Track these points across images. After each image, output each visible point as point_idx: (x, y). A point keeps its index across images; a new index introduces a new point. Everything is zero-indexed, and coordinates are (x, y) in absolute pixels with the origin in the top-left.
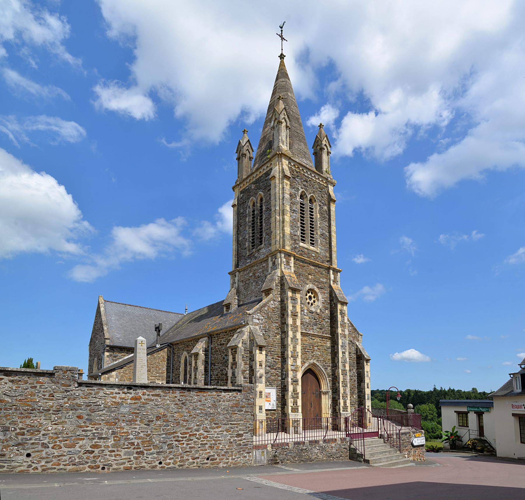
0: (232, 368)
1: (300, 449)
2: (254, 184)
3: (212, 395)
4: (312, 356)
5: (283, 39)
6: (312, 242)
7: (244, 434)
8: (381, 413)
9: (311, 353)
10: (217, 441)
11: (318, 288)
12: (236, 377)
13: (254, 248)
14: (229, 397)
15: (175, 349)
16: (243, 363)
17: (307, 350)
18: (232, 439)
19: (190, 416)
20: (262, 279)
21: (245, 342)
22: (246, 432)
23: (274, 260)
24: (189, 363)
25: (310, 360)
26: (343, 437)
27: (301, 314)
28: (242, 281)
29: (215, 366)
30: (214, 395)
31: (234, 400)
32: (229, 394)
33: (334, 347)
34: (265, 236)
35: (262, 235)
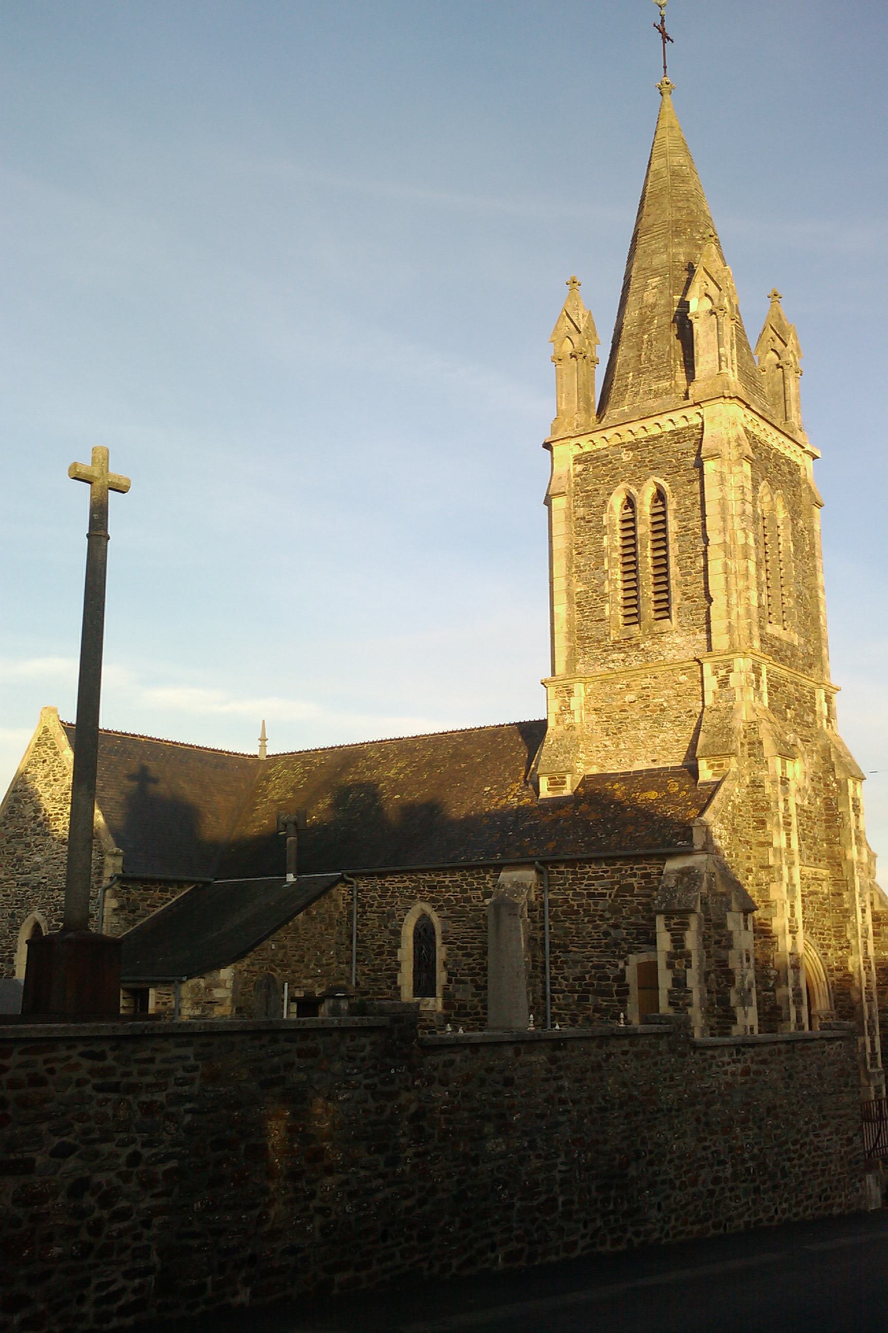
2: (631, 449)
5: (666, 37)
12: (691, 992)
23: (722, 673)
33: (840, 895)
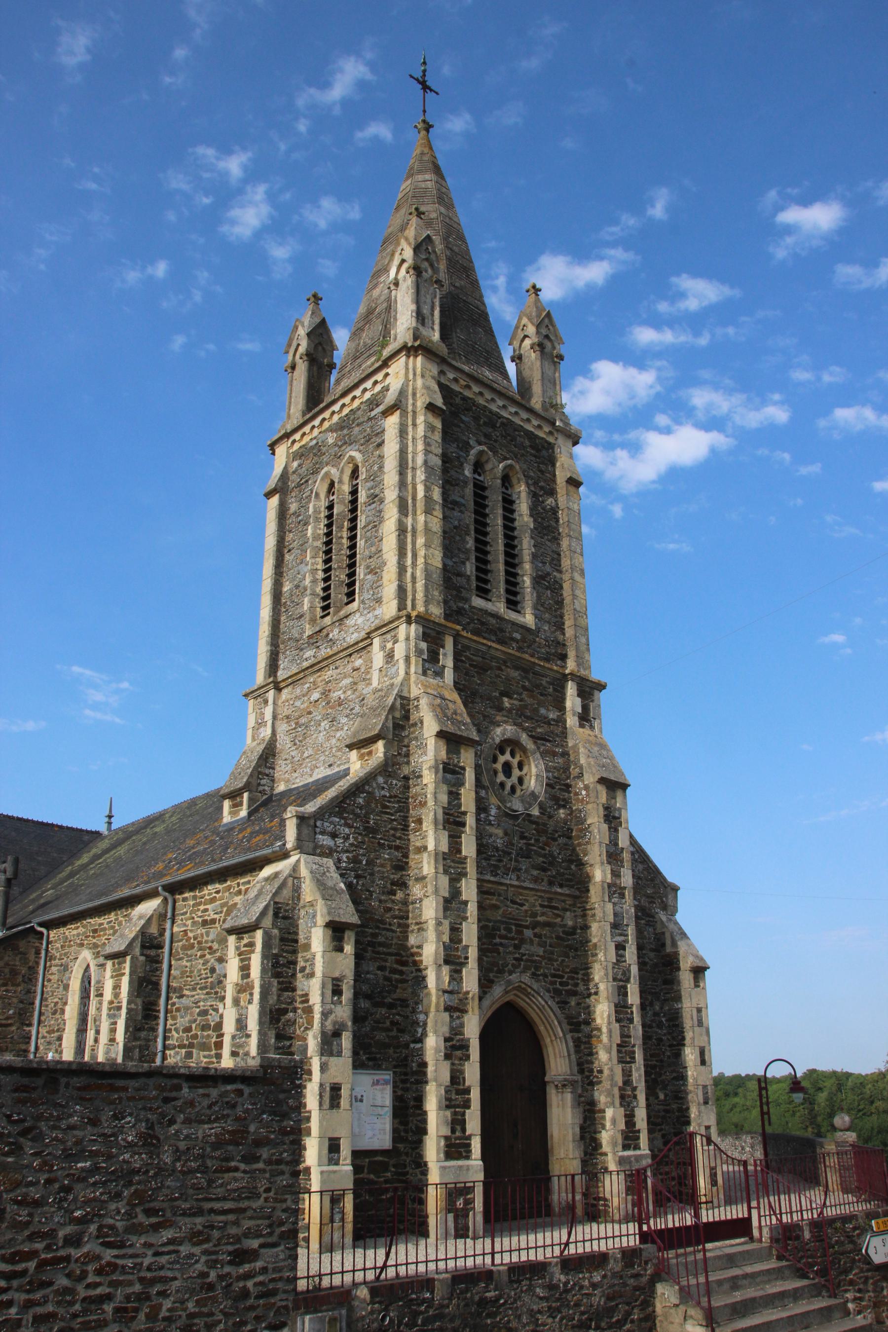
0: (236, 1002)
1: (477, 1298)
2: (336, 431)
3: (141, 1099)
4: (515, 959)
5: (425, 87)
6: (511, 597)
7: (263, 1251)
8: (743, 1148)
9: (511, 949)
10: (153, 1281)
11: (531, 736)
13: (328, 614)
14: (210, 1107)
15: (56, 941)
16: (276, 984)
17: (498, 940)
18: (213, 1275)
19: (49, 1181)
20: (352, 709)
21: (286, 911)
22: (270, 1240)
23: (389, 645)
24: (97, 990)
25: (511, 973)
26: (632, 1243)
27: (478, 820)
28: (288, 717)
29: (182, 996)
30: (150, 1099)
31: (228, 1116)
32: (208, 1095)
34: (362, 577)
35: (355, 575)
